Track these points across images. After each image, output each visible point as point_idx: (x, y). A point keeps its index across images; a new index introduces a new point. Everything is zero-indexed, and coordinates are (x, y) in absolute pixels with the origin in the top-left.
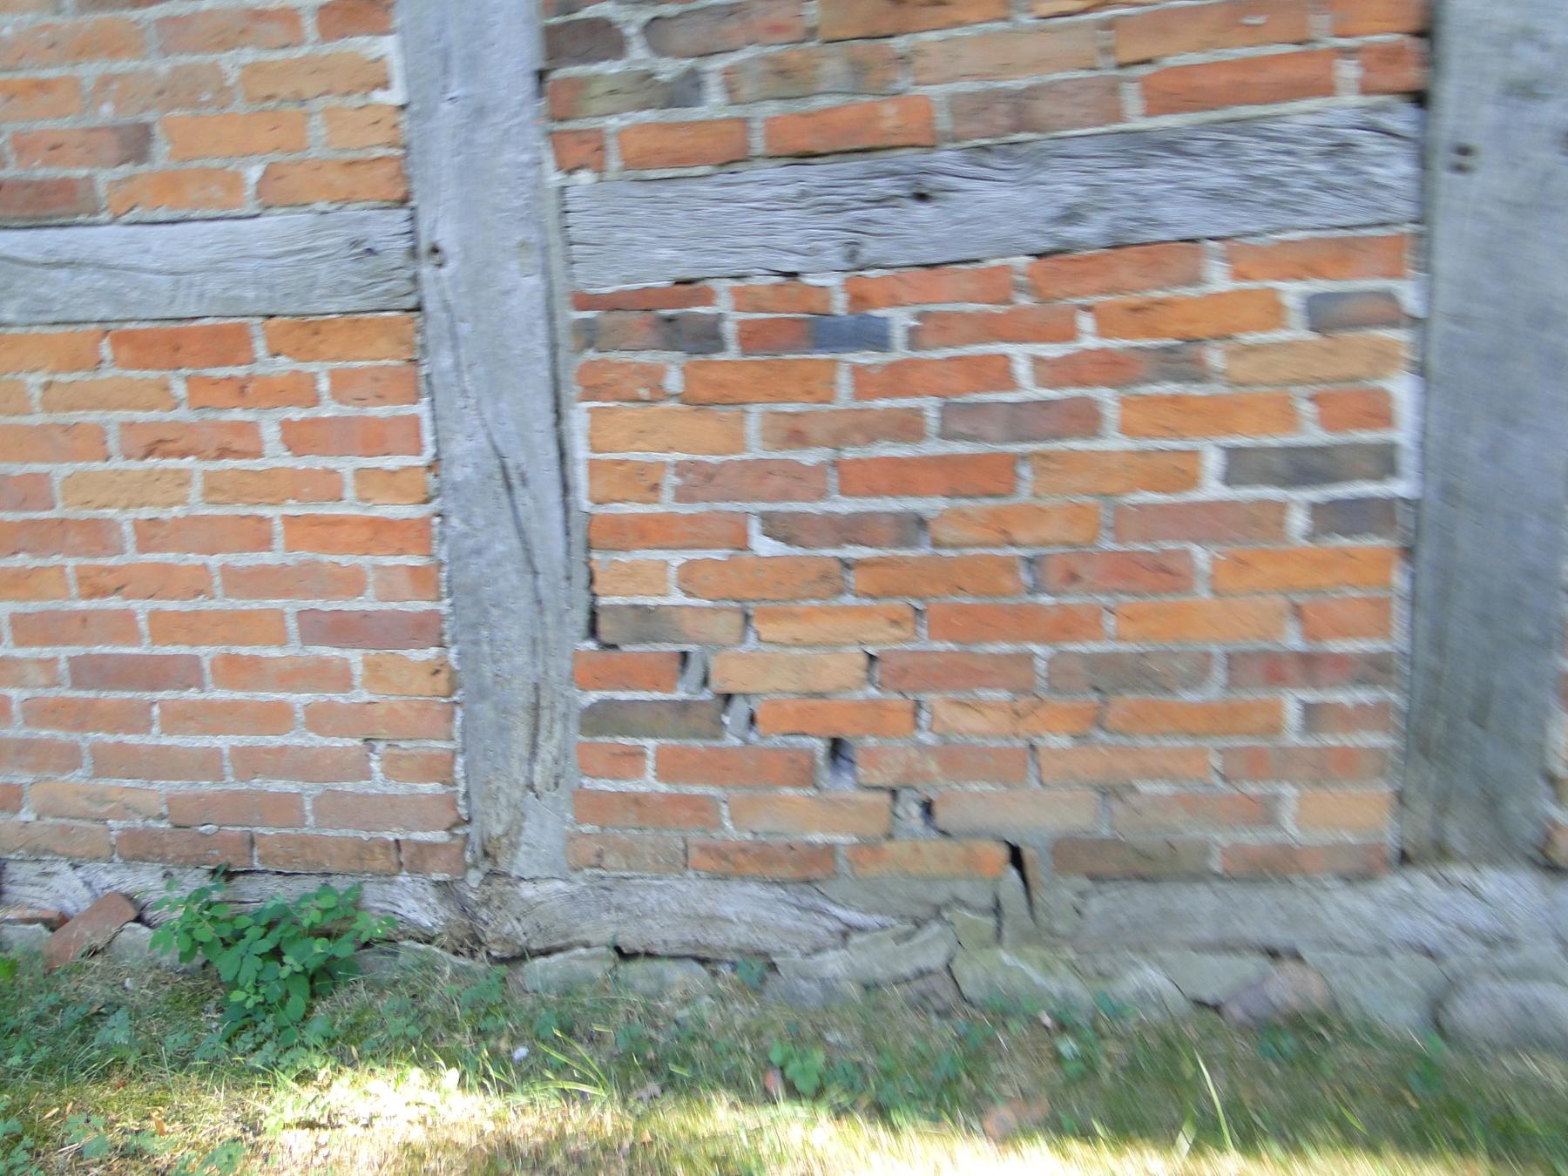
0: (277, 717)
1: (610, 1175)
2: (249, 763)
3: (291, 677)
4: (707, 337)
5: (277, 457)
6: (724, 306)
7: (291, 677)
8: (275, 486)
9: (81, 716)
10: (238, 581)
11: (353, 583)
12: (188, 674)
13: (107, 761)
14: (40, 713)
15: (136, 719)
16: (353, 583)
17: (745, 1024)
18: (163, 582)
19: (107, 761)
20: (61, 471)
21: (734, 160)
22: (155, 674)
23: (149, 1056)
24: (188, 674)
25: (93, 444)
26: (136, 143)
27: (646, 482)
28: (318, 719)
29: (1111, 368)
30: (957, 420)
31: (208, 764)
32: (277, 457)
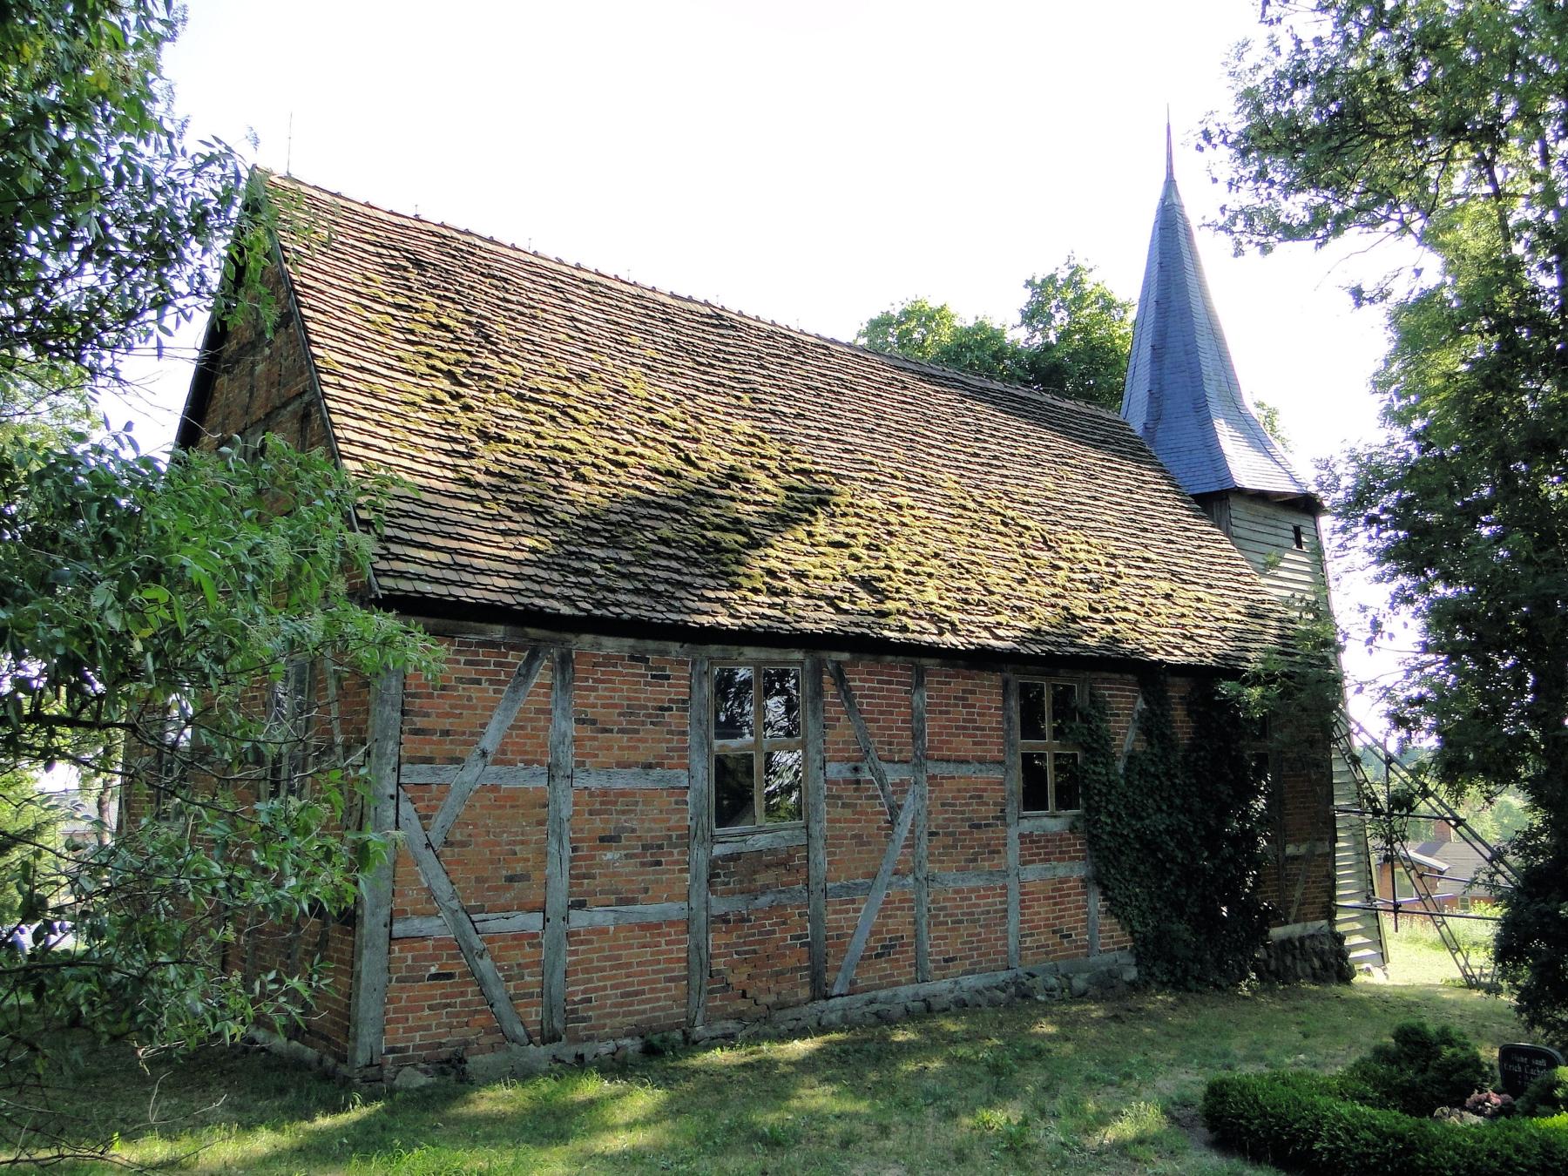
0: (658, 999)
1: (1563, 432)
2: (653, 1010)
3: (662, 990)
4: (728, 922)
5: (664, 947)
6: (731, 917)
7: (662, 990)
8: (662, 953)
9: (621, 1005)
10: (654, 972)
11: (673, 970)
12: (643, 992)
13: (625, 1014)
14: (615, 1005)
15: (631, 1004)
16: (673, 970)
17: (1117, 362)
18: (642, 974)
19: (625, 1014)
20: (624, 953)
21: (734, 894)
22: (637, 993)
23: (1488, 1018)
24: (643, 992)
25: (631, 947)
26: (646, 890)
27: (719, 947)
28: (666, 998)
29: (776, 924)
30: (760, 933)
31: (644, 1012)
32: (664, 947)
